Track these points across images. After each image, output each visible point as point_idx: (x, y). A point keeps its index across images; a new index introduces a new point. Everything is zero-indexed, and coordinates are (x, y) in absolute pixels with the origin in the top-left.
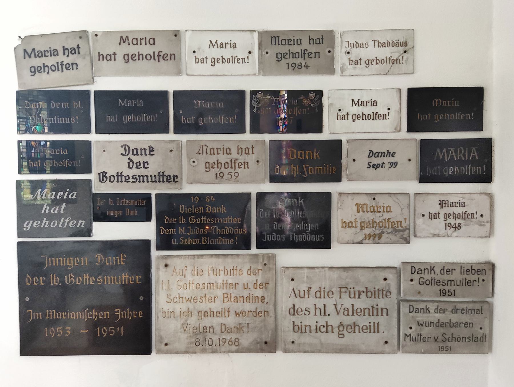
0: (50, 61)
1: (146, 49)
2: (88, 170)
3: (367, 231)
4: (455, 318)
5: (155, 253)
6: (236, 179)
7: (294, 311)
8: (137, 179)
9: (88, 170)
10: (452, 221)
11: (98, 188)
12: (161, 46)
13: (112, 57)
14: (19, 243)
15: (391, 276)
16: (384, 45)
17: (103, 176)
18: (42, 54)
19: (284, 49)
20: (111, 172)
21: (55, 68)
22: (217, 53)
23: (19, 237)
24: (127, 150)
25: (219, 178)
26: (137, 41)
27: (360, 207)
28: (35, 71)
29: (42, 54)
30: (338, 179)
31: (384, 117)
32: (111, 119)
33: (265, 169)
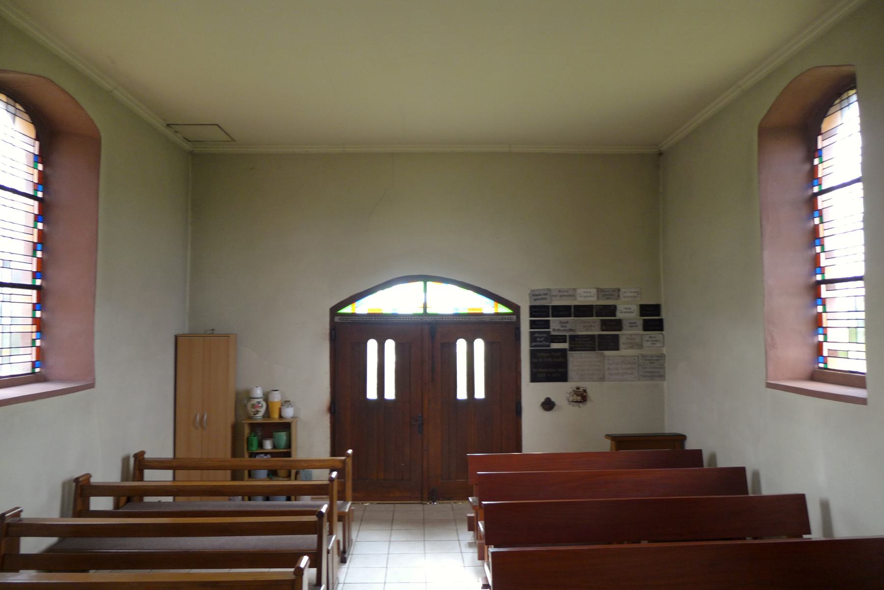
0: (540, 297)
1: (566, 294)
2: (548, 328)
3: (630, 345)
4: (654, 370)
5: (569, 352)
6: (592, 330)
7: (609, 369)
8: (564, 330)
9: (548, 328)
10: (653, 342)
11: (553, 333)
12: (570, 293)
13: (556, 296)
14: (531, 332)
15: (636, 358)
16: (632, 292)
17: (554, 330)
18: (537, 295)
19: (605, 293)
20: (556, 328)
21: (540, 299)
22: (586, 294)
23: (531, 317)
24: (561, 322)
25: (587, 330)
26: (564, 291)
27: (627, 338)
28: (535, 300)
29: (537, 295)
30: (620, 330)
31: (633, 312)
32: (604, 328)
33: (599, 328)
